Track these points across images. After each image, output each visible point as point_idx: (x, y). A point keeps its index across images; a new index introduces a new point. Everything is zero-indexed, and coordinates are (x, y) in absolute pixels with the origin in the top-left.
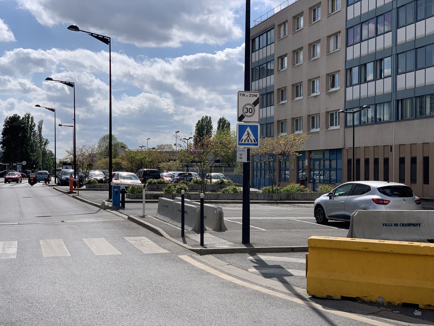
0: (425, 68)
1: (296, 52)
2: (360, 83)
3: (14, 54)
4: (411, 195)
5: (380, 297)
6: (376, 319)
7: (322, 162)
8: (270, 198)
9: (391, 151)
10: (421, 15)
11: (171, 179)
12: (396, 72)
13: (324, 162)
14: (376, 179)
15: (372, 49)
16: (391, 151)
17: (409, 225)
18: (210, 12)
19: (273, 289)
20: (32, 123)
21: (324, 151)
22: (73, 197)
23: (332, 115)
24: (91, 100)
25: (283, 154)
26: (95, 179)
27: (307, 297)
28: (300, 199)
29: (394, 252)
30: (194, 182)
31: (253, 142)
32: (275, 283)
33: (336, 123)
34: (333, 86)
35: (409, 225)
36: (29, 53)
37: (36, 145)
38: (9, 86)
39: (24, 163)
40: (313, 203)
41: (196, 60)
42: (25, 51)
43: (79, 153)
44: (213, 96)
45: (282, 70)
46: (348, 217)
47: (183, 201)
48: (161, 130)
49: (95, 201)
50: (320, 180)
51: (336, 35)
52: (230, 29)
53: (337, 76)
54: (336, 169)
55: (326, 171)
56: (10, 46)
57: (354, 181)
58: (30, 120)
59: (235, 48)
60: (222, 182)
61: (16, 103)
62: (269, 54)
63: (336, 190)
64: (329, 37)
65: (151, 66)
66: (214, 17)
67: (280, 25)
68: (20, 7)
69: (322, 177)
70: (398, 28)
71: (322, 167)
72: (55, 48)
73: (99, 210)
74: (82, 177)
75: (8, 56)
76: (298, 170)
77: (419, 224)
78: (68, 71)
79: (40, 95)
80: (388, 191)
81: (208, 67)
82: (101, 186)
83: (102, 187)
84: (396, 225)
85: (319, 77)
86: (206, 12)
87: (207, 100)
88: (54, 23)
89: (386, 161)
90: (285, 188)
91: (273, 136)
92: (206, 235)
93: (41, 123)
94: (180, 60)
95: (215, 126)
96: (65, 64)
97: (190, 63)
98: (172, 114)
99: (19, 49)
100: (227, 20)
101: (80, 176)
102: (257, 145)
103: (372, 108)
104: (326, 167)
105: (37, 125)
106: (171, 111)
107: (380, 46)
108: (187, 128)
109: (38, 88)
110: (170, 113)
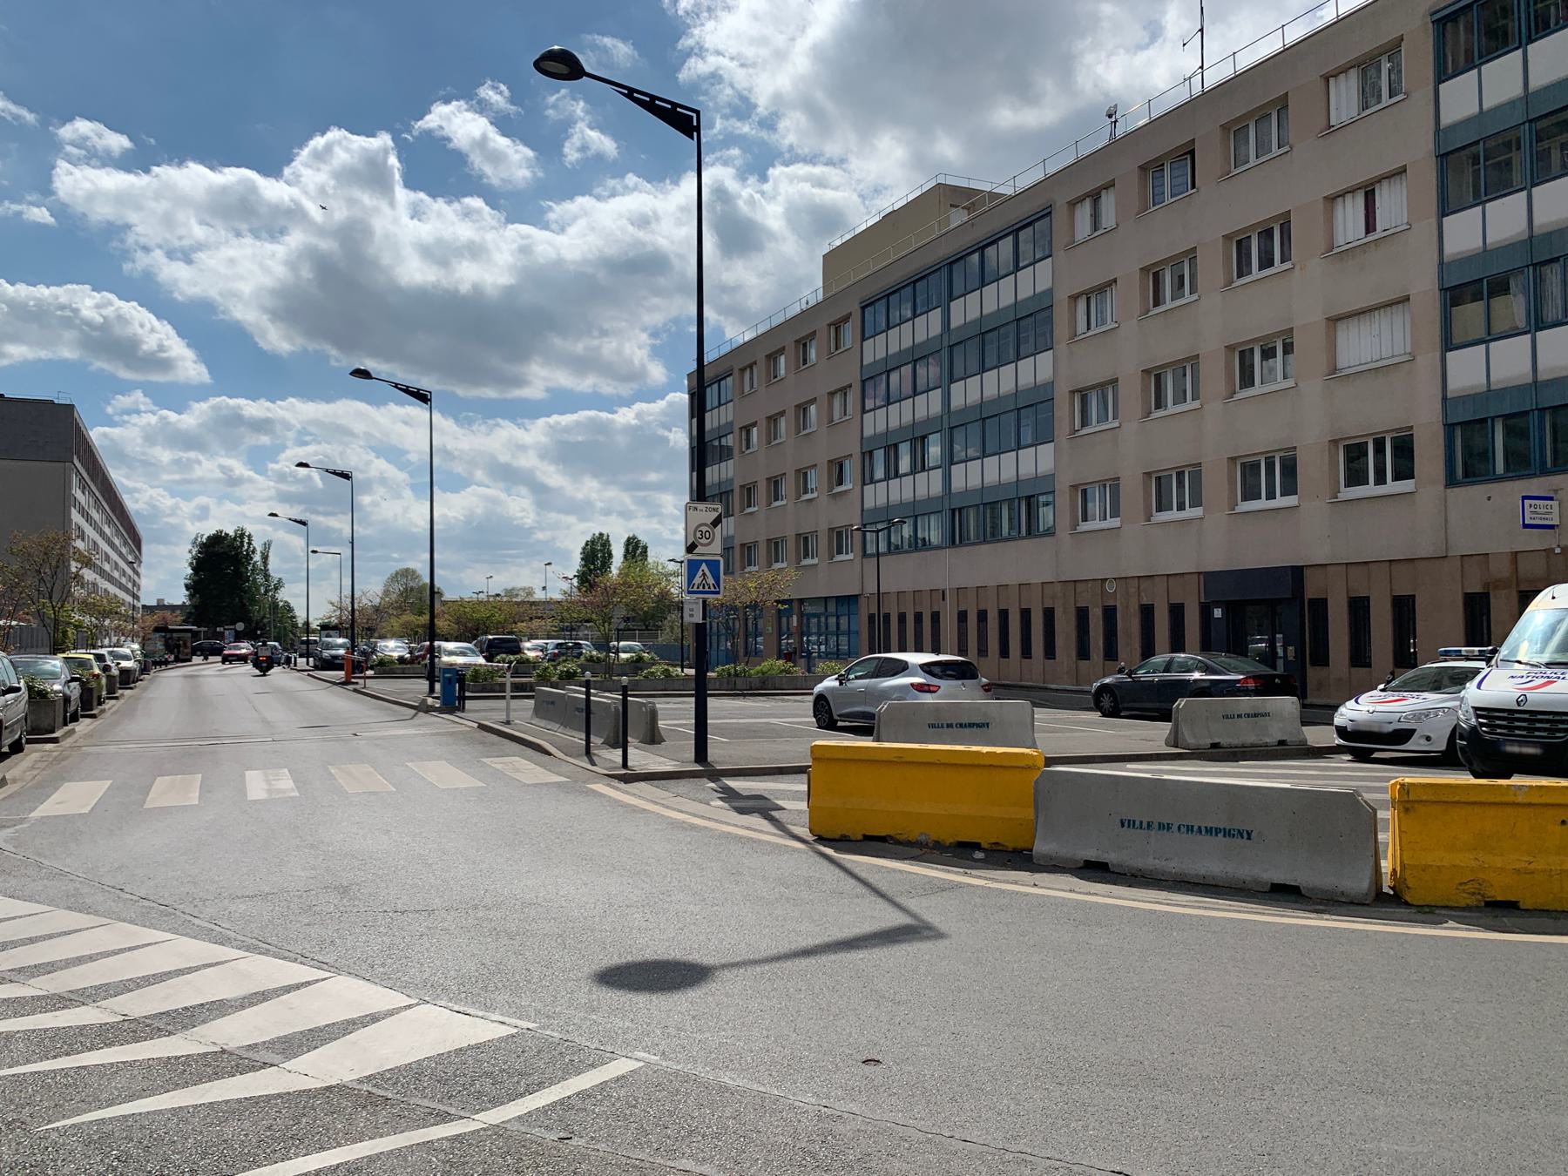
0: (999, 454)
1: (773, 420)
2: (887, 478)
3: (210, 407)
4: (974, 676)
5: (922, 834)
6: (917, 865)
7: (823, 619)
8: (732, 686)
9: (943, 599)
10: (990, 360)
11: (540, 654)
12: (950, 459)
13: (826, 620)
14: (919, 649)
15: (907, 418)
16: (943, 599)
17: (971, 725)
18: (604, 333)
19: (755, 830)
20: (249, 547)
21: (826, 599)
22: (355, 691)
23: (839, 534)
25: (754, 606)
27: (810, 838)
28: (785, 687)
29: (943, 761)
30: (587, 660)
31: (712, 589)
32: (756, 820)
33: (879, 646)
34: (840, 483)
35: (971, 725)
36: (239, 407)
37: (258, 590)
38: (198, 472)
39: (240, 626)
40: (812, 694)
41: (578, 424)
42: (233, 402)
44: (612, 493)
45: (748, 451)
46: (871, 716)
47: (588, 694)
49: (403, 697)
50: (819, 652)
51: (844, 391)
52: (643, 366)
53: (847, 464)
54: (849, 633)
55: (829, 636)
56: (201, 393)
57: (880, 652)
58: (246, 540)
59: (655, 402)
60: (640, 659)
61: (211, 507)
62: (723, 421)
63: (850, 669)
64: (832, 394)
65: (488, 435)
66: (610, 342)
67: (742, 370)
68: (222, 317)
69: (823, 648)
70: (952, 383)
71: (823, 629)
72: (293, 397)
73: (416, 714)
75: (197, 413)
76: (780, 634)
77: (988, 724)
78: (320, 443)
79: (263, 490)
80: (937, 670)
81: (601, 438)
84: (950, 726)
85: (816, 465)
86: (596, 333)
87: (602, 501)
88: (293, 348)
89: (936, 617)
90: (758, 668)
91: (733, 573)
92: (631, 750)
93: (267, 546)
94: (547, 423)
95: (618, 552)
96: (312, 429)
97: (567, 429)
98: (531, 528)
99: (218, 399)
100: (637, 350)
102: (718, 593)
103: (910, 522)
104: (830, 629)
105: (259, 549)
106: (529, 520)
107: (921, 414)
108: (565, 555)
109: (257, 477)
110: (527, 526)
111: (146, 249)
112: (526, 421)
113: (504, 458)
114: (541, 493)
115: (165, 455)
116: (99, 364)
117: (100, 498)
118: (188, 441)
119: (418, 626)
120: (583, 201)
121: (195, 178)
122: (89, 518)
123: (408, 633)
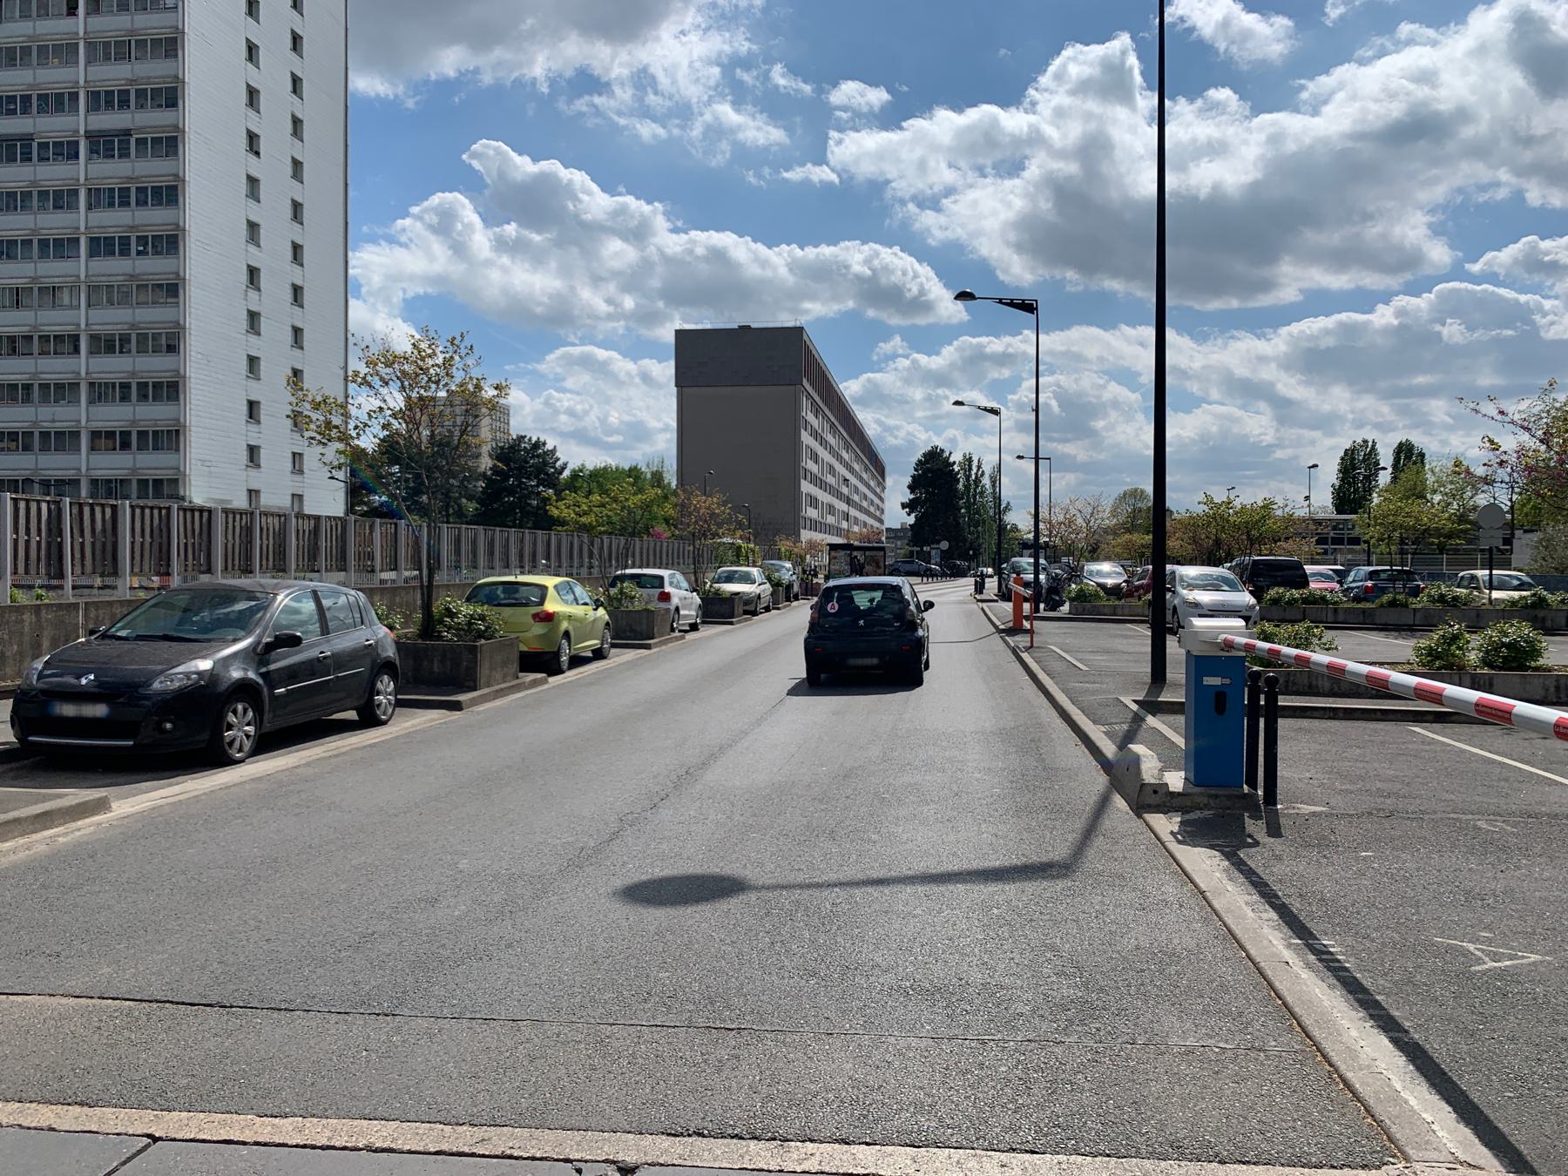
18: (1367, 217)
24: (1100, 424)
26: (1099, 585)
43: (1061, 518)
44: (1367, 402)
48: (1245, 481)
58: (975, 464)
61: (959, 438)
74: (1060, 580)
82: (1115, 607)
83: (1119, 611)
98: (1270, 446)
101: (1052, 578)
111: (903, 202)
112: (1268, 330)
113: (1242, 372)
114: (1284, 409)
115: (918, 394)
116: (871, 313)
117: (836, 423)
118: (940, 379)
119: (1143, 546)
120: (1343, 72)
121: (945, 124)
122: (823, 442)
123: (1126, 556)
